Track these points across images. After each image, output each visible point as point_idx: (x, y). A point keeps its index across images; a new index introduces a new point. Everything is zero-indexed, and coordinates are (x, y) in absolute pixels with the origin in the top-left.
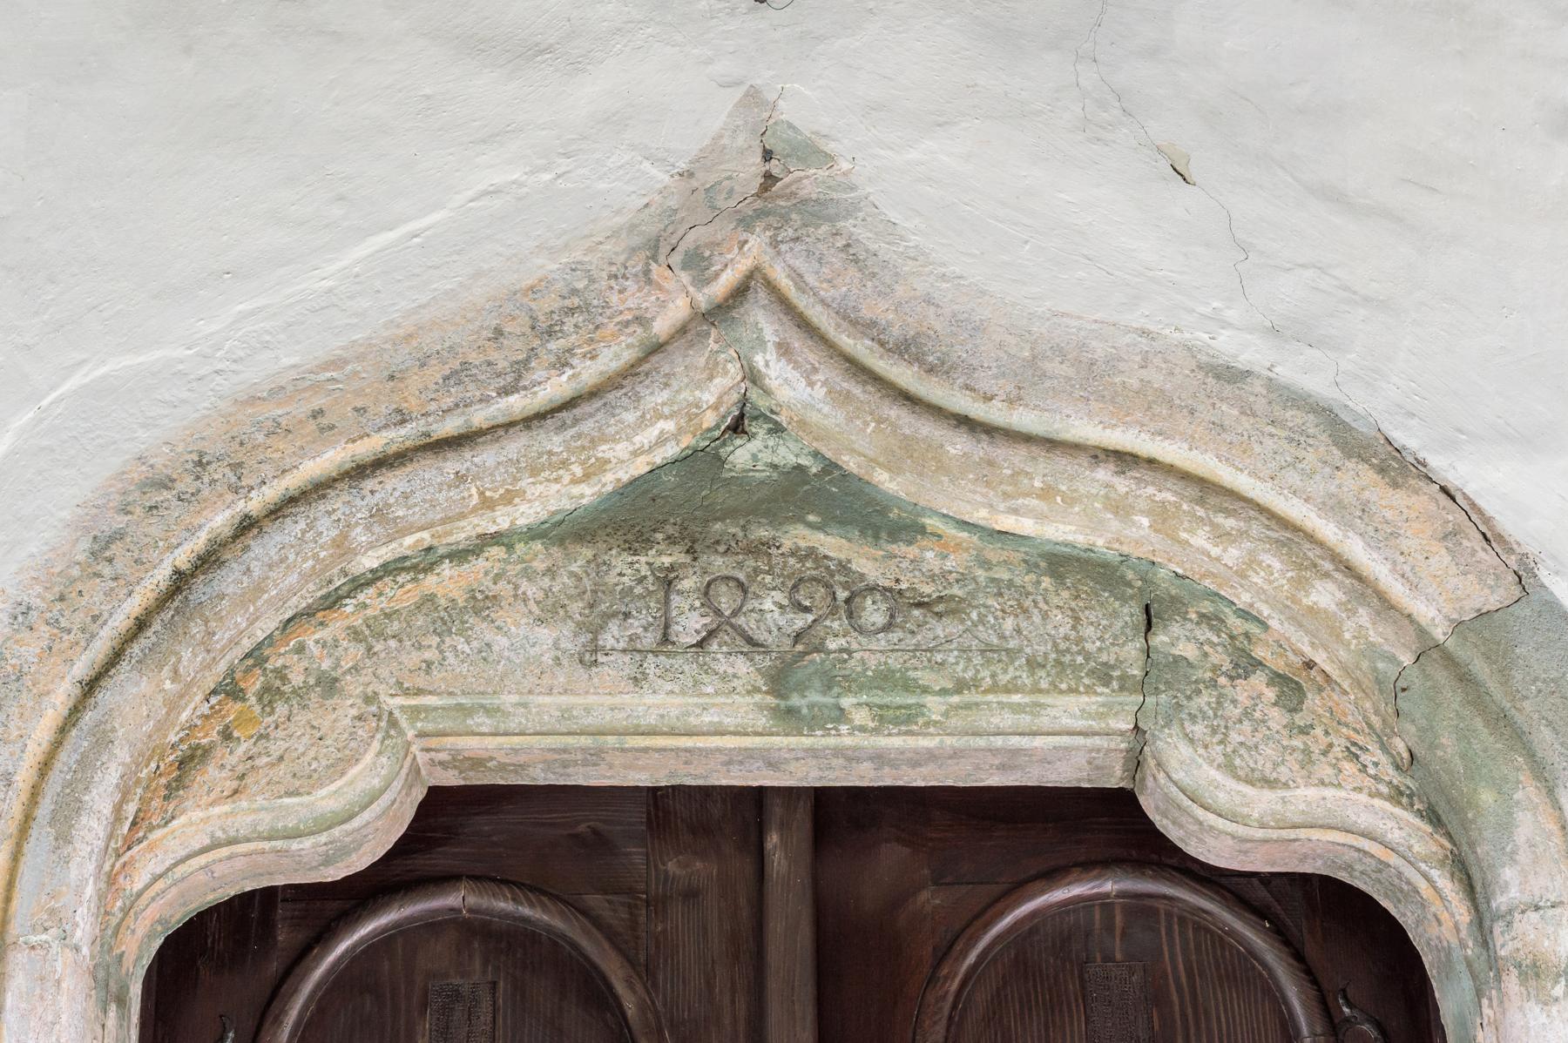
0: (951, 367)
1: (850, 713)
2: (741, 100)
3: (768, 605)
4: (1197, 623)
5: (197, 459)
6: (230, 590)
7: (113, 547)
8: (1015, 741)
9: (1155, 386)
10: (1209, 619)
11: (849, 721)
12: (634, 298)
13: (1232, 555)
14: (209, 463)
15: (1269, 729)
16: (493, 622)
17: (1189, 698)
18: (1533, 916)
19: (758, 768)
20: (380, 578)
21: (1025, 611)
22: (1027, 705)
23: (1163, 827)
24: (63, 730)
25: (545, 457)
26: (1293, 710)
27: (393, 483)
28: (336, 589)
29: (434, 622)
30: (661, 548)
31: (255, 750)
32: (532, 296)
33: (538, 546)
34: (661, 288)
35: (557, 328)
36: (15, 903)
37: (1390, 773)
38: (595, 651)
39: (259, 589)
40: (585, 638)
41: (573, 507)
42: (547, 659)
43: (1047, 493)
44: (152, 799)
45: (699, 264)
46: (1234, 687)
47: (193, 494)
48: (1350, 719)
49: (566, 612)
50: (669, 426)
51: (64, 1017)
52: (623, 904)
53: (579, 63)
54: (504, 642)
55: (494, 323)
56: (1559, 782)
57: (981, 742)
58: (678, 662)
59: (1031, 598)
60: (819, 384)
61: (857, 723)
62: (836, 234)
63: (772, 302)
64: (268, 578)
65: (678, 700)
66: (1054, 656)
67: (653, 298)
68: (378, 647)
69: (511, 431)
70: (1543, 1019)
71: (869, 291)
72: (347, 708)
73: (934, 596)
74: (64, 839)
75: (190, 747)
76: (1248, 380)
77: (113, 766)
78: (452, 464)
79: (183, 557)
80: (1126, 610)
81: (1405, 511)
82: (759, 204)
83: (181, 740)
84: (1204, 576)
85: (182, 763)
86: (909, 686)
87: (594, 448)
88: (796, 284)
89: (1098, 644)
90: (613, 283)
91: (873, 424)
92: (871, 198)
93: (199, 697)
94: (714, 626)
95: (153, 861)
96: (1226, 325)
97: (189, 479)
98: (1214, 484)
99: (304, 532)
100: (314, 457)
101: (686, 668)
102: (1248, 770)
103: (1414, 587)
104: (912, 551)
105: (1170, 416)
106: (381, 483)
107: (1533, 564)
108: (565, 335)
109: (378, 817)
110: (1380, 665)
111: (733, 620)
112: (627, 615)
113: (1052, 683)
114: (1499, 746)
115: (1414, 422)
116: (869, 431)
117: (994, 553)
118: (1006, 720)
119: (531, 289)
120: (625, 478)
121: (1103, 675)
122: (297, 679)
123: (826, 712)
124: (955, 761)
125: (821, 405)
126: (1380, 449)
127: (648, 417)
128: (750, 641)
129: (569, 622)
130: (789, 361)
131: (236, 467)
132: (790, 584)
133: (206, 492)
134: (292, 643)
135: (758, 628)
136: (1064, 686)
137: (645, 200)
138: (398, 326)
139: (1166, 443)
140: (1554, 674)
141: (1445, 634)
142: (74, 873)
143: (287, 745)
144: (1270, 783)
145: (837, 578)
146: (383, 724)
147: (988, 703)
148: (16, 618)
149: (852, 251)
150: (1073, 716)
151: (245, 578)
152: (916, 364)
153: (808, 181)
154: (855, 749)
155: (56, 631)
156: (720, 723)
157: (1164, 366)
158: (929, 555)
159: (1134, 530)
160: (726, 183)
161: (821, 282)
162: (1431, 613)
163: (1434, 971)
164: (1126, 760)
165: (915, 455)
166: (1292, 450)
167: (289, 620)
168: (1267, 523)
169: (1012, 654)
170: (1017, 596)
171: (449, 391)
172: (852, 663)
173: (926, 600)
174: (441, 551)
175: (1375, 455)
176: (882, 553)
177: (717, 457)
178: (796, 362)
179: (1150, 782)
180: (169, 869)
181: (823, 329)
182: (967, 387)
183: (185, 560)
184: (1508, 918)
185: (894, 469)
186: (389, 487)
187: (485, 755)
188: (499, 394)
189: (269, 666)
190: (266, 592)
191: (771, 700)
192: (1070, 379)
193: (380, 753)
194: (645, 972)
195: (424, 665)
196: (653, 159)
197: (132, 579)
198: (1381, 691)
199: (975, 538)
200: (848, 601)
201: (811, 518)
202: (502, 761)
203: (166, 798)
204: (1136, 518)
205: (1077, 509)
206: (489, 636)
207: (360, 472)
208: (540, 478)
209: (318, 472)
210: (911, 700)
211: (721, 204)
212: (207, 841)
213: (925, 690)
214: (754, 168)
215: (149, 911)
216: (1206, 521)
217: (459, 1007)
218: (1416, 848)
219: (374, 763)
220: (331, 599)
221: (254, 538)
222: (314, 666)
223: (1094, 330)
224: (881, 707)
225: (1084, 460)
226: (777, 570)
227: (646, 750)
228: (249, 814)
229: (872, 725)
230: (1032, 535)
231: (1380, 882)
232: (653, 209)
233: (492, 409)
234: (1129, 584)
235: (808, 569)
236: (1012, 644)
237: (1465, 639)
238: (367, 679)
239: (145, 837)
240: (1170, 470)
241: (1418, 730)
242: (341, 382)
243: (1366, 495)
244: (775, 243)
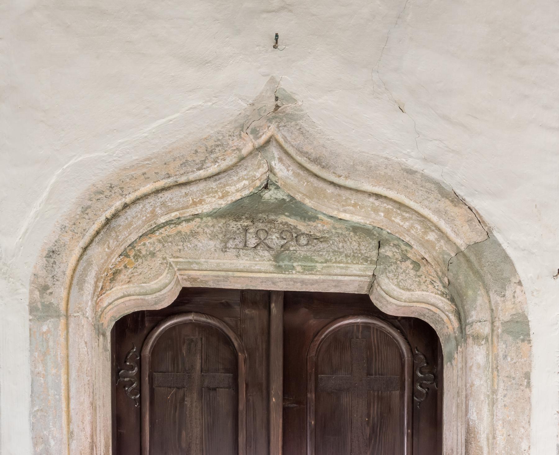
0: (329, 167)
1: (296, 267)
2: (268, 81)
3: (274, 237)
4: (393, 247)
5: (110, 186)
6: (122, 224)
7: (88, 210)
8: (340, 278)
9: (389, 174)
10: (396, 245)
11: (295, 270)
12: (236, 142)
13: (406, 225)
14: (113, 187)
15: (410, 275)
16: (197, 239)
17: (389, 267)
18: (479, 324)
19: (270, 284)
20: (166, 226)
21: (345, 241)
22: (344, 267)
23: (376, 304)
24: (78, 261)
25: (211, 189)
26: (417, 271)
27: (167, 195)
28: (154, 228)
29: (181, 239)
30: (244, 220)
31: (133, 271)
32: (206, 141)
33: (209, 218)
34: (244, 140)
35: (214, 151)
36: (69, 306)
37: (442, 289)
38: (226, 248)
39: (130, 224)
40: (223, 244)
41: (219, 207)
42: (213, 250)
43: (355, 205)
44: (106, 283)
45: (255, 132)
46: (401, 264)
47: (109, 196)
48: (432, 274)
49: (218, 237)
50: (246, 182)
51: (85, 335)
52: (234, 320)
53: (219, 67)
54: (201, 245)
55: (195, 148)
56: (491, 290)
57: (330, 278)
58: (249, 252)
59: (347, 238)
60: (290, 170)
61: (298, 270)
62: (297, 125)
63: (277, 145)
64: (133, 221)
65: (249, 262)
66: (352, 254)
67: (242, 143)
68: (166, 245)
69: (201, 181)
70: (478, 349)
71: (306, 143)
72: (158, 261)
73: (320, 236)
74: (81, 289)
75: (116, 270)
76: (416, 174)
77: (93, 271)
78: (184, 190)
79: (108, 214)
80: (373, 242)
81: (457, 213)
82: (274, 115)
83: (113, 268)
84: (396, 233)
85: (114, 274)
86: (312, 261)
87: (225, 187)
88: (284, 140)
89: (365, 251)
90: (230, 137)
91: (306, 183)
92: (308, 114)
93: (117, 256)
94: (259, 243)
95: (108, 299)
96: (411, 157)
97: (108, 191)
98: (403, 204)
99: (142, 208)
100: (144, 187)
101: (251, 253)
102: (403, 286)
103: (457, 235)
104: (315, 224)
105: (392, 183)
106: (163, 195)
107: (492, 230)
108: (216, 153)
109: (169, 292)
110: (445, 256)
111: (264, 241)
112: (235, 239)
113: (352, 261)
114: (476, 279)
115: (463, 188)
116: (304, 185)
117: (338, 225)
118: (338, 271)
119: (206, 139)
120: (234, 200)
121: (366, 259)
122: (144, 252)
123: (289, 267)
124: (323, 284)
125: (291, 177)
126: (452, 195)
127: (240, 179)
128: (269, 247)
129: (219, 240)
130: (282, 163)
131: (122, 188)
132: (280, 232)
133: (113, 195)
134: (142, 243)
135: (271, 243)
136: (355, 262)
137: (240, 112)
138: (167, 148)
139: (390, 192)
140: (493, 260)
141: (464, 248)
142: (85, 299)
143: (142, 270)
144: (409, 290)
145: (293, 231)
146: (168, 265)
147: (334, 266)
148: (62, 229)
149: (301, 130)
150: (357, 270)
151: (126, 221)
152: (319, 165)
153: (288, 107)
154: (296, 279)
155: (73, 233)
156: (260, 269)
157: (391, 168)
158: (319, 225)
159: (379, 217)
160: (264, 108)
161: (292, 140)
162: (461, 243)
163: (443, 342)
164: (369, 285)
165: (318, 193)
166: (427, 195)
167: (141, 236)
168: (418, 215)
169: (341, 253)
170: (343, 237)
171: (182, 168)
172: (297, 254)
173: (318, 237)
174: (182, 219)
175: (451, 197)
176: (306, 224)
177: (260, 196)
178: (284, 164)
179: (375, 291)
180: (113, 302)
181: (292, 155)
182: (334, 173)
183: (109, 215)
184: (471, 324)
185: (311, 198)
186: (166, 196)
187: (197, 277)
188: (197, 170)
189: (136, 249)
190: (133, 225)
191: (274, 263)
192: (364, 171)
193: (167, 273)
194: (240, 336)
195: (179, 250)
196: (243, 100)
197: (94, 219)
198: (444, 264)
199: (332, 221)
200: (296, 237)
201: (286, 214)
202: (201, 279)
203: (110, 283)
204: (380, 213)
205: (363, 210)
206: (196, 243)
207: (157, 192)
208: (209, 196)
209: (145, 191)
210: (313, 265)
211: (262, 114)
212: (122, 295)
213: (317, 262)
214: (272, 103)
215: (109, 313)
216: (400, 214)
217: (193, 343)
218: (446, 308)
219: (166, 276)
220: (152, 231)
221: (128, 209)
222: (149, 249)
223: (371, 157)
224: (304, 266)
225: (366, 195)
226: (277, 228)
227: (240, 277)
228: (132, 288)
229: (301, 271)
230: (349, 220)
231: (432, 319)
232: (242, 115)
233: (195, 174)
234: (375, 235)
235: (285, 228)
236: (341, 250)
237: (470, 250)
238: (163, 253)
239: (105, 293)
240: (391, 200)
241: (453, 274)
242: (151, 165)
243: (447, 208)
244: (278, 127)
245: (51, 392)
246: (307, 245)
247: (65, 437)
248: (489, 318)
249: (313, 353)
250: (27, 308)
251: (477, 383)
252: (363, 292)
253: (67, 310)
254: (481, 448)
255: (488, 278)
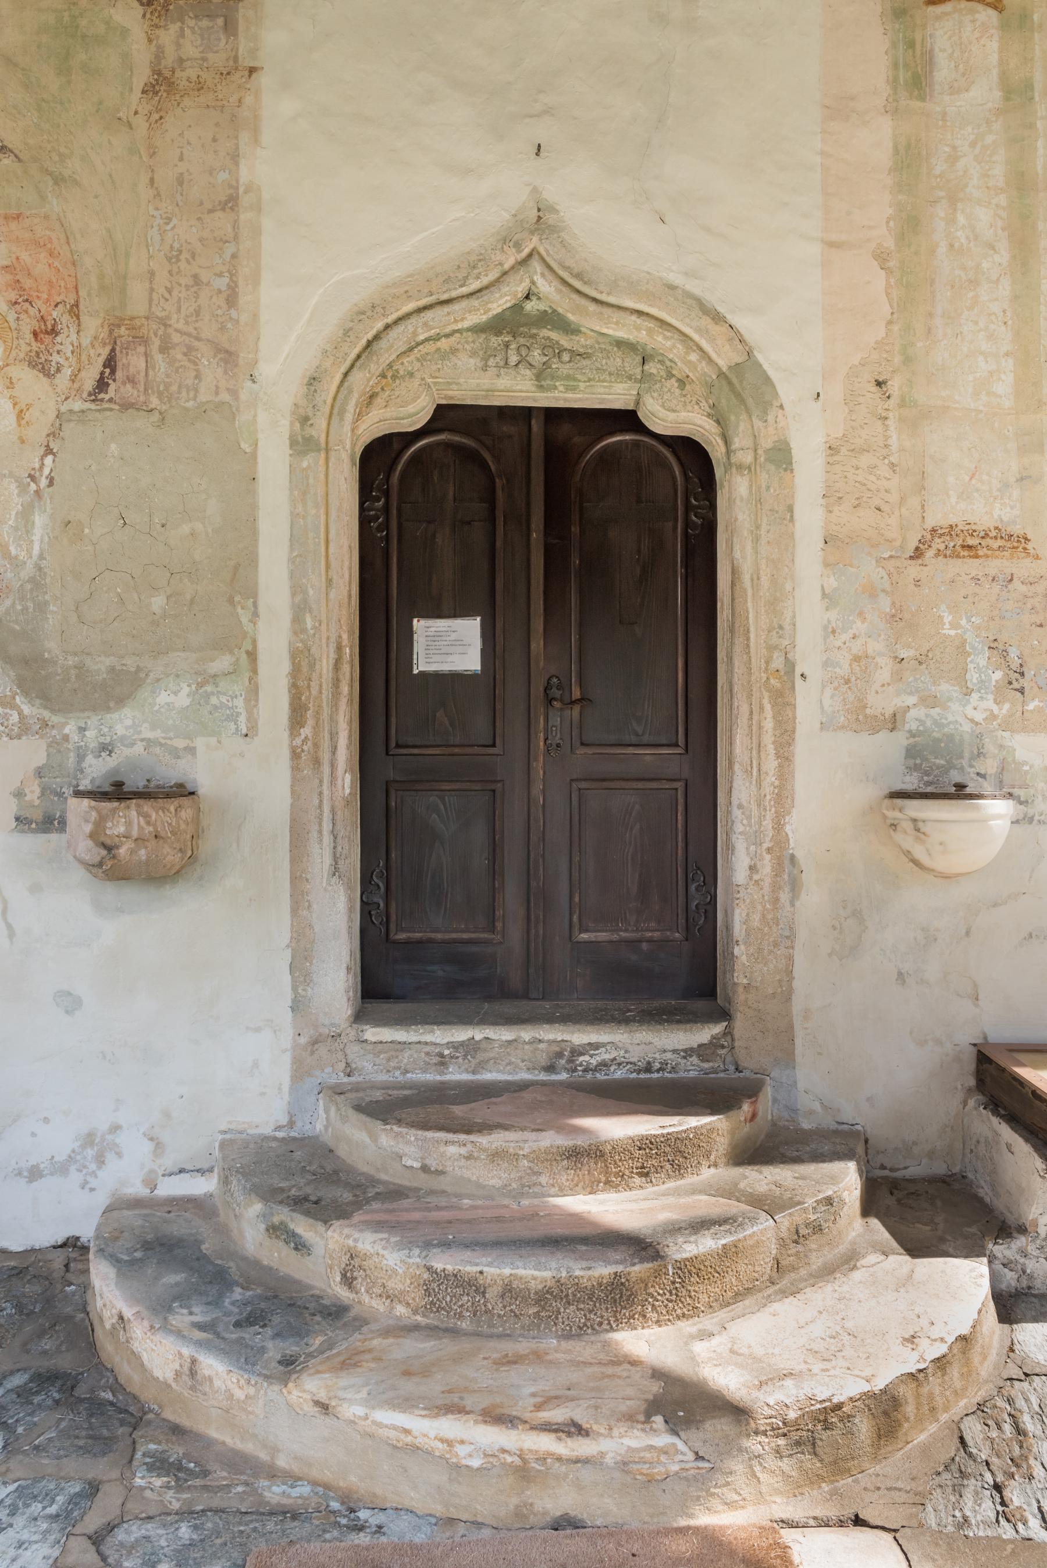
12: (498, 257)
13: (669, 344)
27: (429, 315)
33: (470, 333)
39: (392, 346)
43: (617, 323)
45: (518, 246)
50: (508, 298)
58: (510, 371)
72: (416, 382)
74: (342, 419)
78: (446, 309)
79: (370, 336)
86: (575, 380)
103: (719, 355)
104: (577, 338)
118: (602, 390)
122: (402, 373)
131: (384, 308)
144: (674, 411)
153: (550, 219)
162: (723, 363)
207: (420, 310)
225: (628, 313)
244: (541, 240)
245: (311, 535)
246: (570, 361)
247: (324, 585)
248: (752, 445)
249: (577, 478)
250: (288, 442)
251: (740, 517)
252: (631, 407)
253: (327, 443)
254: (745, 590)
255: (750, 401)
